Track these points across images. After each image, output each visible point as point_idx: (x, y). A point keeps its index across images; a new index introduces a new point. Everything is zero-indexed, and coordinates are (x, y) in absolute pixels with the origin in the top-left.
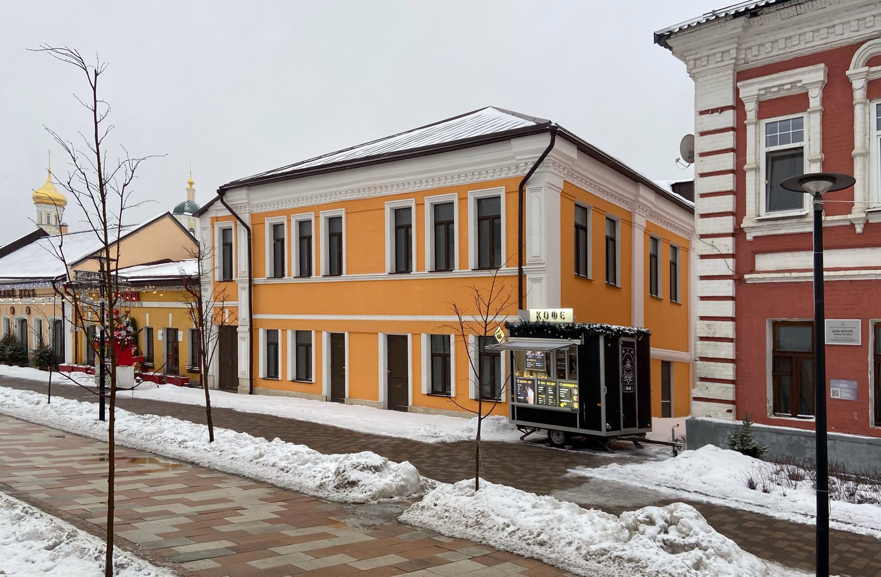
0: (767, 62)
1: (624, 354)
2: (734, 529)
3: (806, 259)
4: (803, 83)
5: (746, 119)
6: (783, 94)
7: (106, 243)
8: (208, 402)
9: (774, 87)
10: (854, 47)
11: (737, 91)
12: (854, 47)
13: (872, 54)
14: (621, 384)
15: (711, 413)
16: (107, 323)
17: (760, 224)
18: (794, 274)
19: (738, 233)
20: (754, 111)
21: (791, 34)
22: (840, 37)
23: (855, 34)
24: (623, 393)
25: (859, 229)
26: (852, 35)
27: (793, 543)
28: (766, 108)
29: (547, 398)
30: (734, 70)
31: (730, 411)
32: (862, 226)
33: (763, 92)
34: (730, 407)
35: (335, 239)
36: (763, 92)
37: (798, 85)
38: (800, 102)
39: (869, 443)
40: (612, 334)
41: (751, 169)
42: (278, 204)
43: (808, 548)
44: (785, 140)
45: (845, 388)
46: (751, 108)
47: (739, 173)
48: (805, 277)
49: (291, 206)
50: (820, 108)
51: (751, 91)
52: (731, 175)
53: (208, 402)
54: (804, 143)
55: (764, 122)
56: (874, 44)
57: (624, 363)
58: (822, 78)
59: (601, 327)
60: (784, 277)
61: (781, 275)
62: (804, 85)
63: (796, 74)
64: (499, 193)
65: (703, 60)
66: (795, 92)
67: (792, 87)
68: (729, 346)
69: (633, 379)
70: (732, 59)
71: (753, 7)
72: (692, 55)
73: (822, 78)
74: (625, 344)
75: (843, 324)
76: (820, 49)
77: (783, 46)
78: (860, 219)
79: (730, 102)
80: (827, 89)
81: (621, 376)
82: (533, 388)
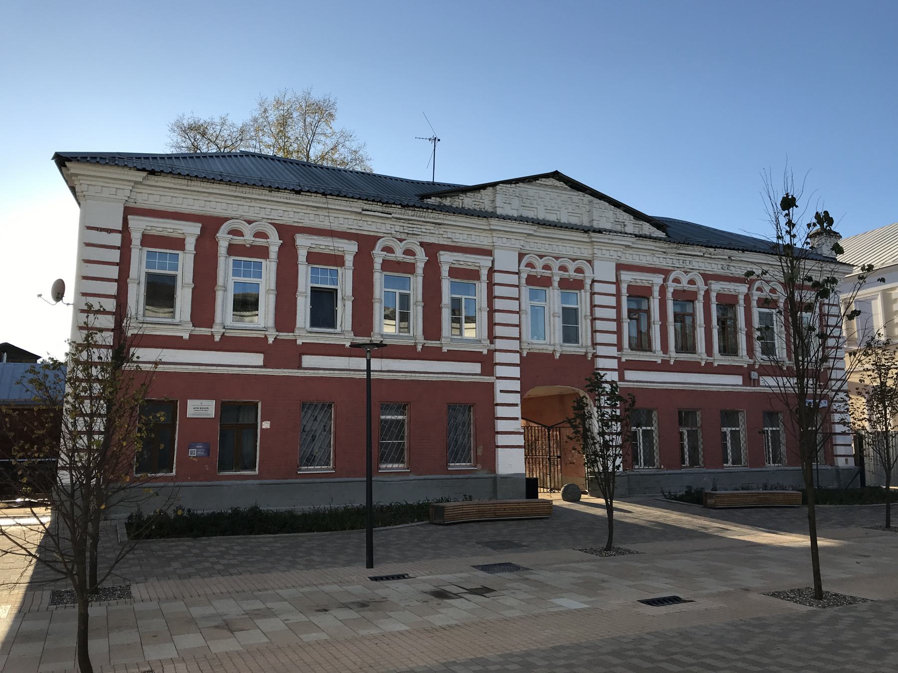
0: (153, 207)
3: (361, 363)
7: (836, 324)
10: (226, 219)
12: (226, 219)
16: (79, 501)
18: (702, 386)
19: (118, 330)
22: (213, 210)
23: (222, 211)
26: (222, 211)
32: (220, 337)
33: (149, 228)
38: (178, 244)
43: (68, 589)
45: (200, 448)
46: (136, 238)
51: (138, 225)
54: (179, 273)
55: (146, 249)
71: (478, 210)
72: (87, 180)
75: (201, 403)
76: (197, 213)
80: (199, 240)
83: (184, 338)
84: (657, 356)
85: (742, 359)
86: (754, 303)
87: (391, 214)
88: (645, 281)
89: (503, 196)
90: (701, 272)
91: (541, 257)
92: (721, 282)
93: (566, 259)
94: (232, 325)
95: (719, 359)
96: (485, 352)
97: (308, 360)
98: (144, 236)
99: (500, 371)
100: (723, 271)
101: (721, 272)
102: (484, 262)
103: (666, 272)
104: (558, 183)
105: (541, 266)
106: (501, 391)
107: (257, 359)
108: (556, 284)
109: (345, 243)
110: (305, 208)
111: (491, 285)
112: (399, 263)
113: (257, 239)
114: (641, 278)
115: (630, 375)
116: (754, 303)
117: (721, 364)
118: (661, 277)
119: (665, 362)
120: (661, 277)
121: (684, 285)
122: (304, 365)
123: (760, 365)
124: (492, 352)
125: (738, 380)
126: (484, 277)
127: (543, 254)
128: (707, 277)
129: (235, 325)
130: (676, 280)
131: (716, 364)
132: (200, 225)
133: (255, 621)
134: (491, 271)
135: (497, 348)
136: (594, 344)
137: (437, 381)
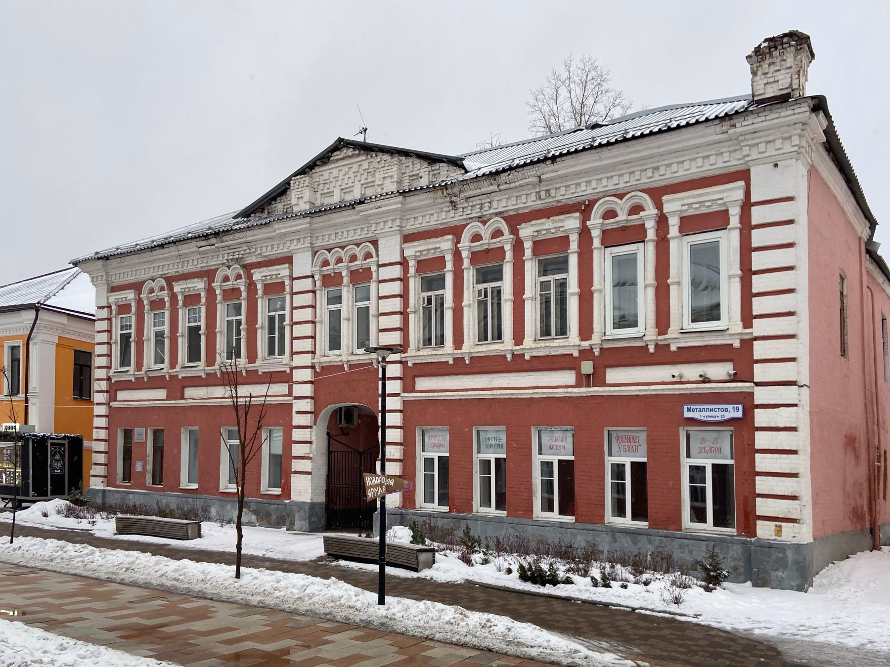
1: (52, 451)
2: (613, 632)
4: (725, 200)
5: (524, 256)
6: (704, 210)
8: (239, 547)
9: (709, 201)
11: (402, 251)
13: (607, 208)
14: (49, 469)
15: (96, 484)
17: (183, 369)
20: (451, 262)
21: (501, 197)
24: (52, 475)
25: (652, 350)
27: (700, 649)
28: (690, 224)
29: (10, 479)
30: (108, 286)
31: (102, 482)
34: (102, 479)
35: (16, 363)
36: (686, 207)
37: (720, 202)
39: (144, 494)
40: (36, 439)
41: (675, 283)
42: (10, 331)
44: (195, 321)
47: (404, 314)
48: (442, 396)
49: (11, 334)
50: (577, 250)
52: (398, 316)
53: (239, 547)
56: (631, 197)
57: (53, 455)
58: (578, 225)
59: (30, 435)
60: (604, 391)
61: (204, 401)
62: (725, 203)
63: (125, 294)
64: (187, 328)
65: (512, 199)
66: (559, 234)
67: (547, 233)
68: (397, 448)
69: (64, 466)
73: (578, 225)
74: (52, 444)
77: (514, 202)
78: (651, 341)
79: (398, 259)
81: (49, 463)
82: (5, 473)
83: (734, 345)
84: (447, 352)
86: (651, 234)
87: (214, 245)
88: (697, 206)
89: (297, 190)
90: (163, 276)
91: (358, 245)
92: (533, 222)
93: (352, 246)
94: (690, 327)
95: (531, 345)
96: (737, 344)
97: (189, 392)
98: (535, 243)
99: (760, 372)
100: (539, 202)
101: (538, 205)
102: (733, 193)
103: (456, 231)
104: (350, 152)
105: (626, 211)
106: (298, 413)
107: (161, 394)
108: (346, 280)
109: (196, 282)
111: (747, 227)
112: (624, 229)
113: (607, 221)
114: (548, 227)
115: (422, 383)
116: (651, 234)
117: (417, 362)
118: (448, 240)
119: (662, 348)
120: (448, 240)
121: (487, 242)
122: (186, 396)
123: (657, 345)
124: (748, 344)
126: (735, 221)
127: (330, 247)
128: (515, 221)
129: (695, 327)
130: (610, 214)
131: (673, 348)
133: (398, 648)
134: (747, 205)
135: (756, 334)
136: (748, 318)
137: (669, 394)
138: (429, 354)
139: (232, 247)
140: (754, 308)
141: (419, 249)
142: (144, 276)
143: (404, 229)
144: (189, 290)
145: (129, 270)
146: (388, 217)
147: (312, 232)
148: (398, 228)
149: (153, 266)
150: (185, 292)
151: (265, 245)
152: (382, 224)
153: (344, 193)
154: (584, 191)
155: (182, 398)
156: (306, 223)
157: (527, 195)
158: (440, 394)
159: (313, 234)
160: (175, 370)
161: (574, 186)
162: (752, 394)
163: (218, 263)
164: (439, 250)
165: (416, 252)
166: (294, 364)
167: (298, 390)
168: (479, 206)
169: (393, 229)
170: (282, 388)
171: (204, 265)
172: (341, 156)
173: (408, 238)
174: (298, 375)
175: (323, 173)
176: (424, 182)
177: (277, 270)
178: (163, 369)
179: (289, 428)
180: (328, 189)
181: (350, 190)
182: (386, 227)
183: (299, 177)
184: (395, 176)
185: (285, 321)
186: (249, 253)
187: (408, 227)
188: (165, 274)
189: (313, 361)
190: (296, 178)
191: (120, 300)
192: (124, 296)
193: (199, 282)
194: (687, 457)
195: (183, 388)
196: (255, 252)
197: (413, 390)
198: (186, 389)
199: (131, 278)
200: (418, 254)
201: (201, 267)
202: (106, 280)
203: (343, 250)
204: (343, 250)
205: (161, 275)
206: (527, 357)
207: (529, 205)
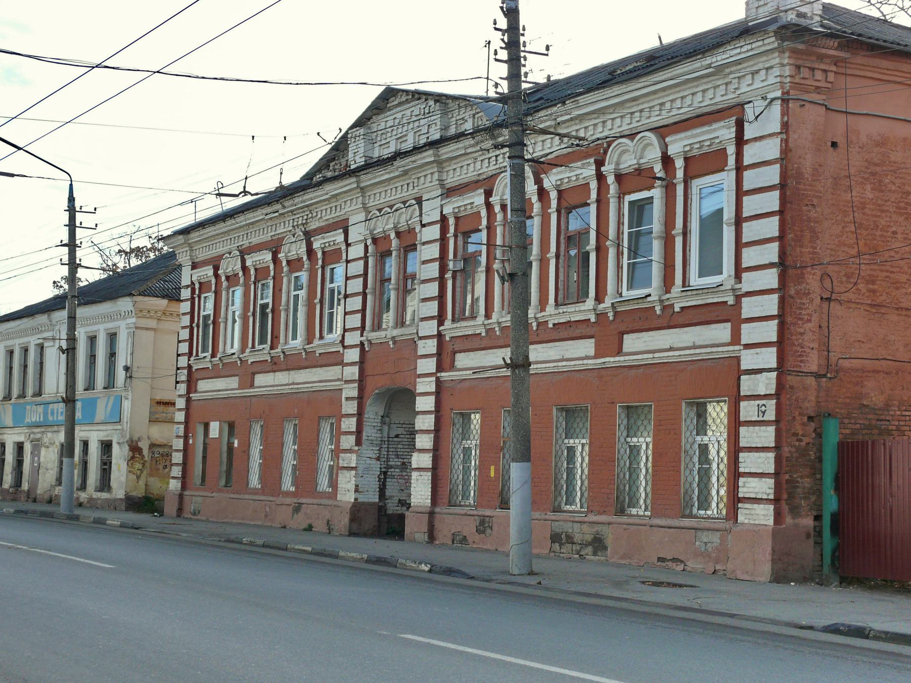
35: (93, 358)
63: (715, 130)
66: (715, 148)
70: (776, 77)
85: (585, 310)
87: (278, 212)
110: (327, 202)
111: (740, 169)
125: (587, 347)
126: (732, 161)
132: (212, 267)
136: (739, 271)
138: (465, 328)
139: (295, 212)
140: (437, 306)
141: (456, 205)
142: (223, 249)
143: (445, 182)
144: (466, 209)
145: (210, 243)
146: (697, 86)
147: (440, 163)
148: (778, 79)
149: (230, 237)
150: (201, 279)
151: (429, 172)
152: (422, 178)
153: (401, 142)
154: (593, 131)
155: (619, 352)
156: (430, 156)
157: (739, 78)
158: (543, 365)
159: (192, 247)
160: (311, 345)
161: (737, 80)
162: (738, 359)
163: (285, 230)
164: (717, 141)
165: (454, 208)
166: (745, 287)
167: (749, 333)
168: (657, 108)
169: (433, 184)
170: (721, 332)
171: (273, 233)
172: (396, 102)
173: (449, 192)
174: (750, 307)
175: (381, 123)
176: (468, 126)
177: (334, 236)
178: (650, 295)
179: (736, 400)
180: (386, 139)
181: (405, 139)
182: (456, 175)
183: (355, 130)
184: (439, 123)
185: (674, 228)
186: (312, 217)
187: (449, 181)
188: (241, 246)
189: (363, 338)
190: (352, 131)
191: (462, 209)
192: (205, 273)
193: (267, 253)
194: (22, 443)
195: (254, 374)
196: (316, 216)
197: (452, 367)
198: (625, 336)
199: (396, 197)
200: (456, 210)
201: (271, 236)
202: (190, 255)
203: (632, 141)
204: (632, 141)
205: (238, 247)
206: (677, 309)
207: (644, 122)
